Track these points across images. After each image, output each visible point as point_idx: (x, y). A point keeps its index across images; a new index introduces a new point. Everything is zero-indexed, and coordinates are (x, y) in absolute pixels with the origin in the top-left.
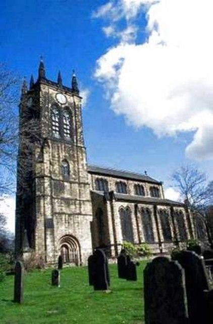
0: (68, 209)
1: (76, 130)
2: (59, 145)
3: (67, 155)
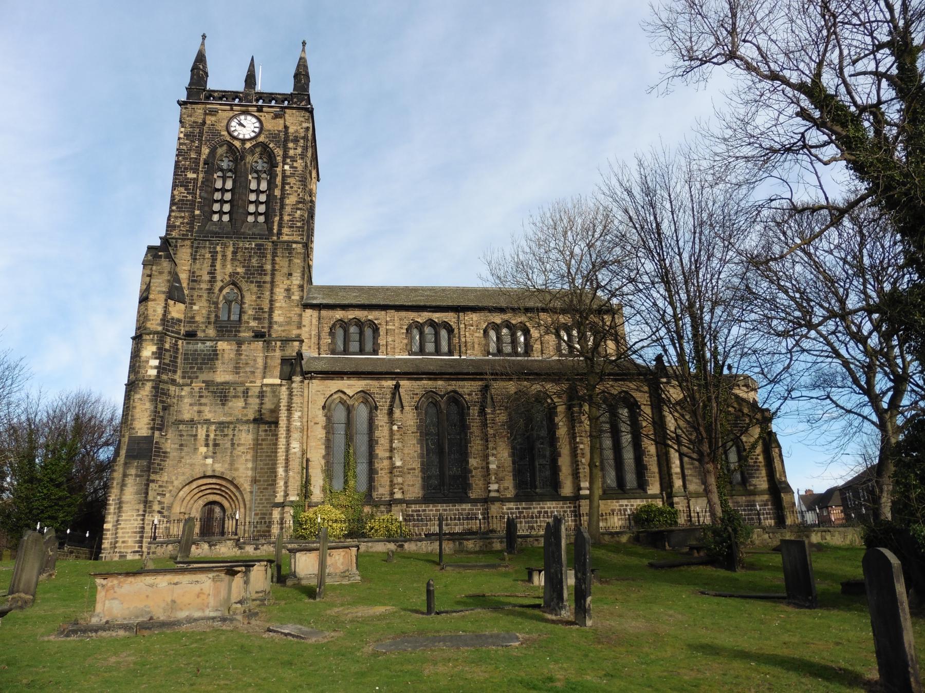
0: (219, 409)
1: (283, 198)
2: (186, 221)
3: (240, 270)
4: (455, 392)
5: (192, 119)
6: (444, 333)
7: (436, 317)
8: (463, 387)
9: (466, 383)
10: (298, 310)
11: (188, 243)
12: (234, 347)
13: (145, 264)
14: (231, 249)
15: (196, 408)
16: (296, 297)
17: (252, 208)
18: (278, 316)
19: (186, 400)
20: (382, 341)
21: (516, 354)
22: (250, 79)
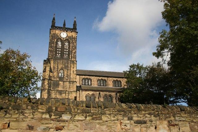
4: (111, 95)
5: (53, 33)
6: (90, 81)
7: (103, 78)
8: (112, 94)
9: (91, 92)
10: (75, 76)
11: (53, 60)
12: (63, 83)
13: (44, 64)
14: (61, 61)
15: (55, 95)
16: (75, 73)
17: (65, 53)
18: (71, 76)
19: (53, 94)
20: (92, 83)
21: (88, 85)
22: (64, 25)
